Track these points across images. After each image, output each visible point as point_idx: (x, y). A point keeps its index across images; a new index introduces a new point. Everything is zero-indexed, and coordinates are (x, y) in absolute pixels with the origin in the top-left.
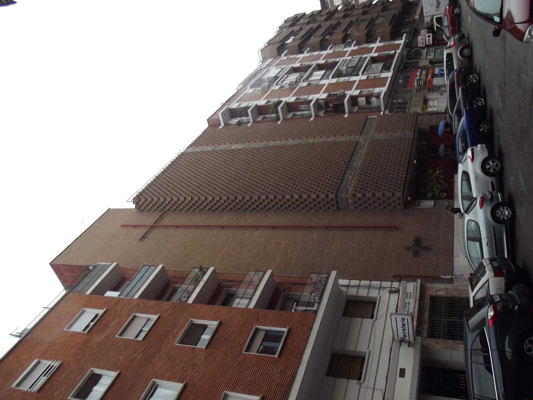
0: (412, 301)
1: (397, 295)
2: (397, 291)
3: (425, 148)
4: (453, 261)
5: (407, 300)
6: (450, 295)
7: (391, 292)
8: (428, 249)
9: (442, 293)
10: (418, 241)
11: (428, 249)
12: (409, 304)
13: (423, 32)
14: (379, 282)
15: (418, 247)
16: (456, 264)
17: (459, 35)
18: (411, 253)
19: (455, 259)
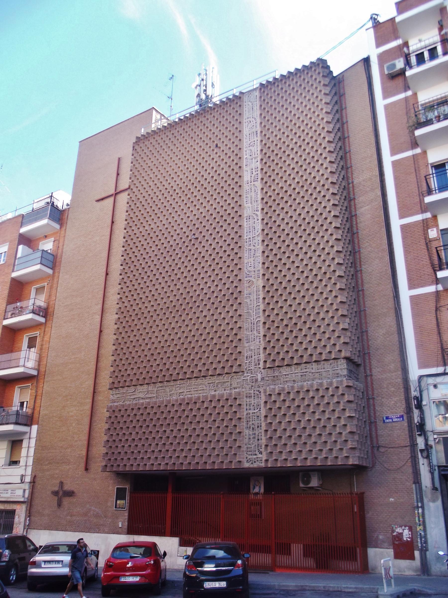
0: (8, 495)
1: (20, 482)
2: (22, 482)
3: (301, 485)
4: (45, 529)
5: (10, 491)
6: (15, 526)
7: (22, 476)
8: (59, 504)
9: (16, 519)
10: (70, 494)
11: (59, 504)
12: (7, 493)
13: (311, 485)
14: (31, 464)
15: (63, 494)
16: (42, 532)
17: (118, 577)
18: (56, 489)
19: (47, 532)
